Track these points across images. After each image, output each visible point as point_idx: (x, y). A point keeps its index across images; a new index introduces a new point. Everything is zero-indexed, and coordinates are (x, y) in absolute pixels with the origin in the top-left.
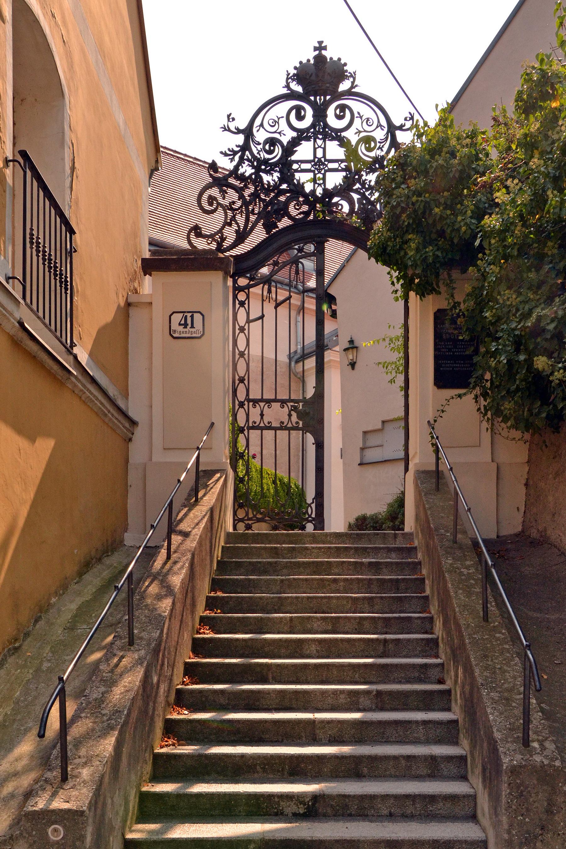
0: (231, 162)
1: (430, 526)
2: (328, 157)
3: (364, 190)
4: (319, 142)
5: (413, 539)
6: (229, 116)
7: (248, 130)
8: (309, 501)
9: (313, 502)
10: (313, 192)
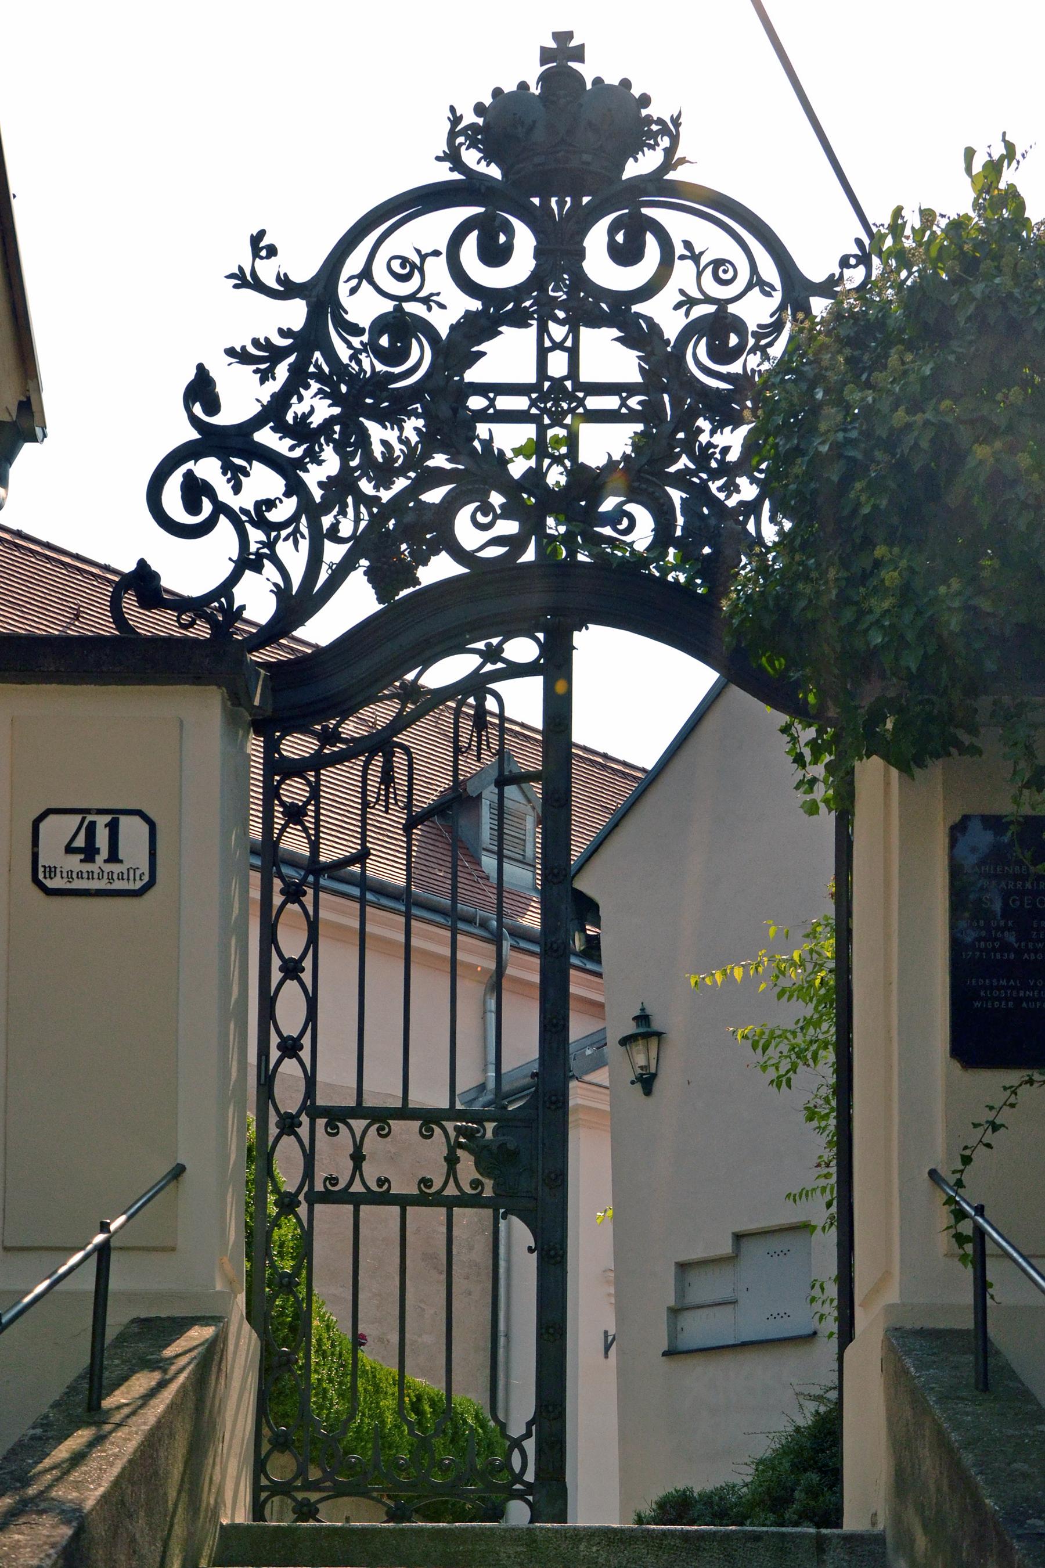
0: (263, 381)
1: (978, 1505)
2: (585, 377)
3: (704, 476)
4: (558, 331)
5: (884, 1554)
6: (256, 240)
7: (320, 288)
8: (516, 1430)
9: (528, 1435)
10: (535, 477)
